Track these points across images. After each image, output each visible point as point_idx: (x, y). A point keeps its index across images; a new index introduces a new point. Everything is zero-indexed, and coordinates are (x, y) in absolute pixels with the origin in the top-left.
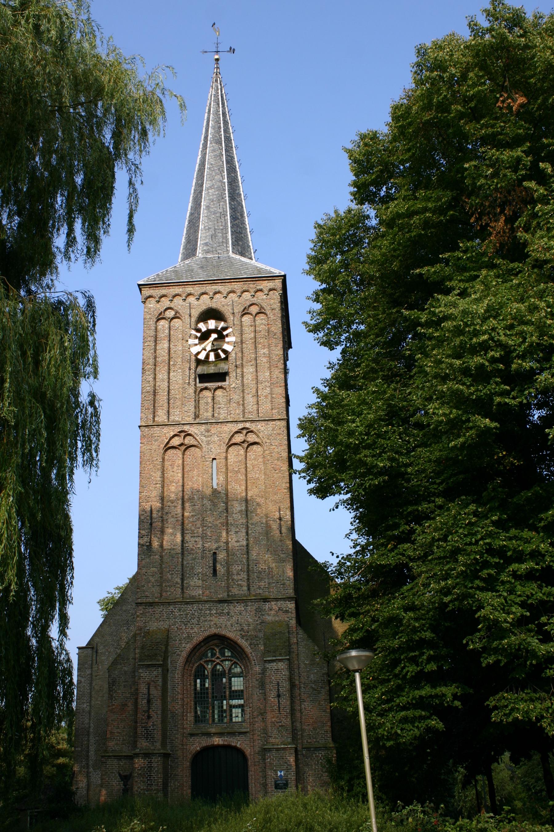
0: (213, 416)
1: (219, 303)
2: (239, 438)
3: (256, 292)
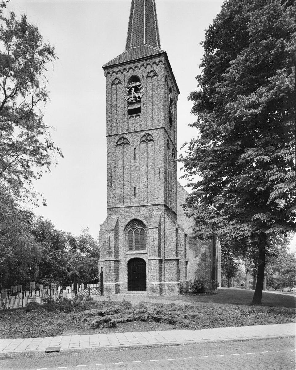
0: (135, 129)
1: (137, 73)
2: (144, 138)
3: (153, 64)
